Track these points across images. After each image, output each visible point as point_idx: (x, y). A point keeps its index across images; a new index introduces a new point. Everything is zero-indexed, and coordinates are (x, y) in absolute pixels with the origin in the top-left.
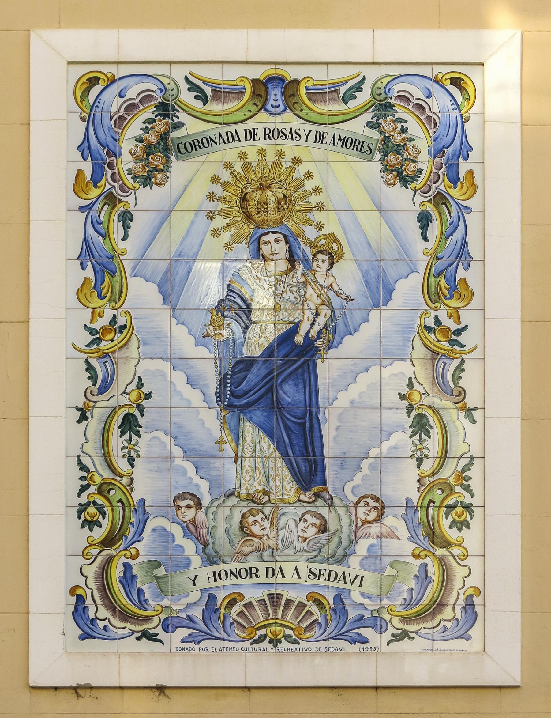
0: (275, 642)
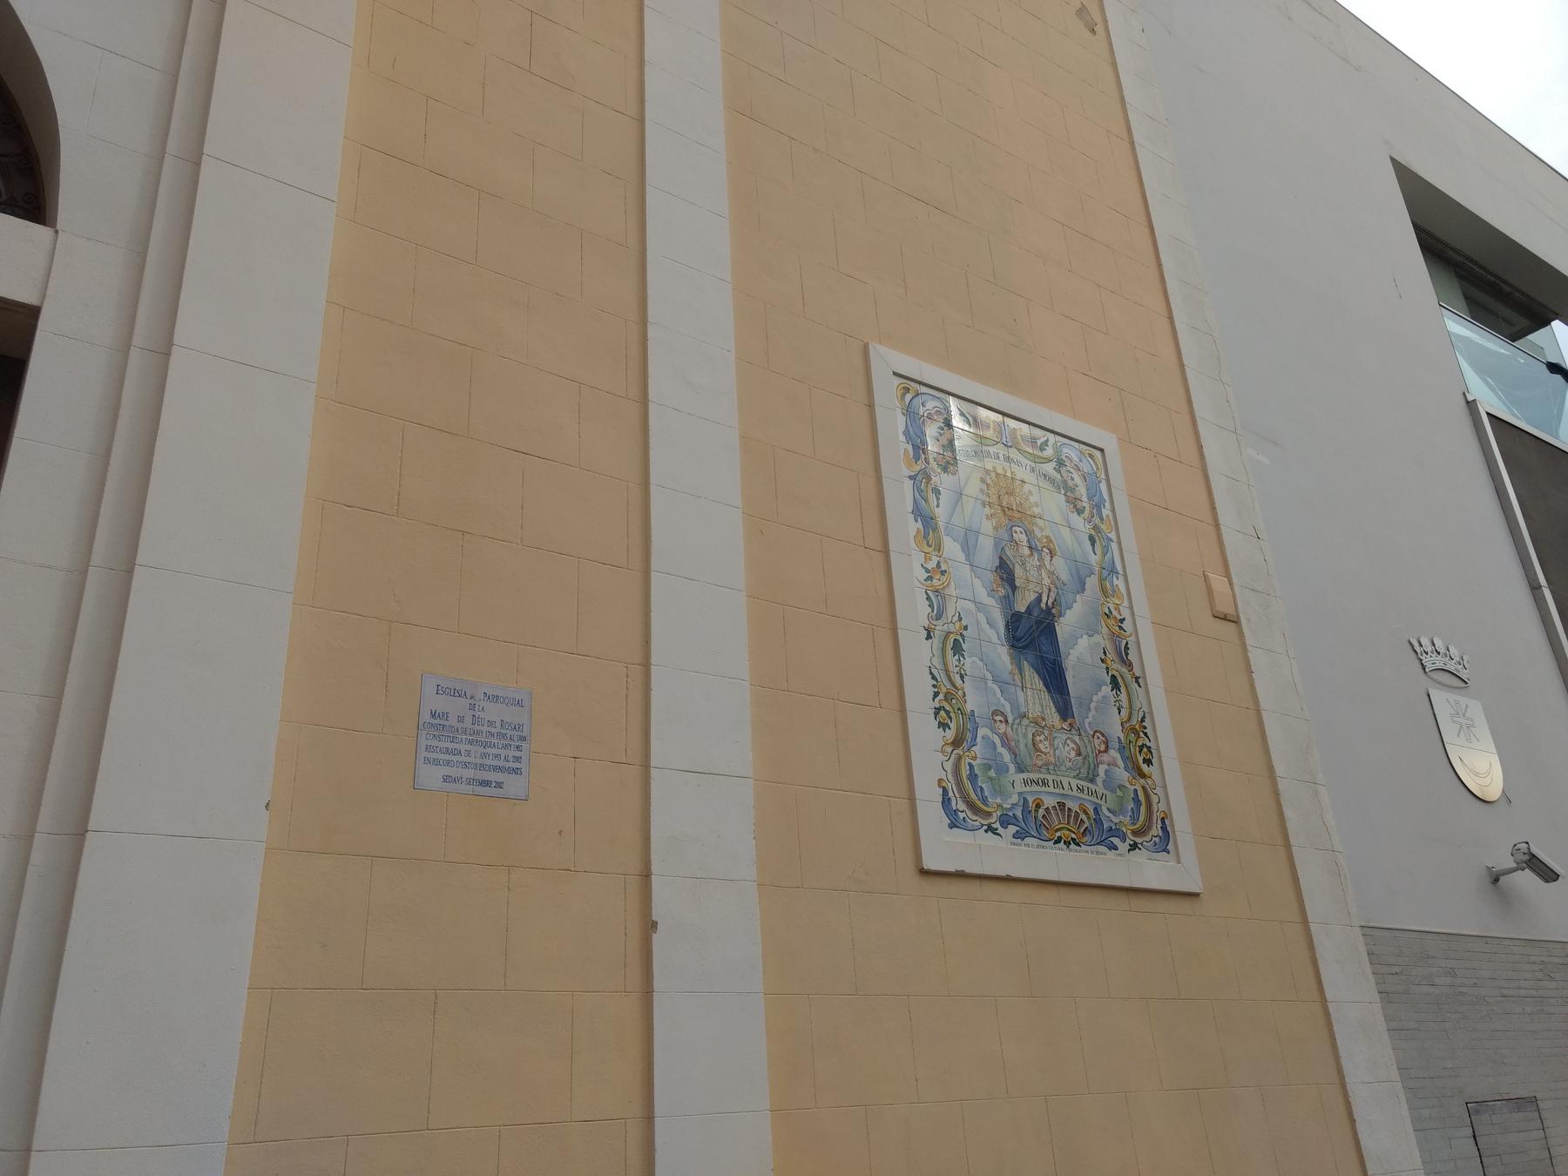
0: (1067, 844)
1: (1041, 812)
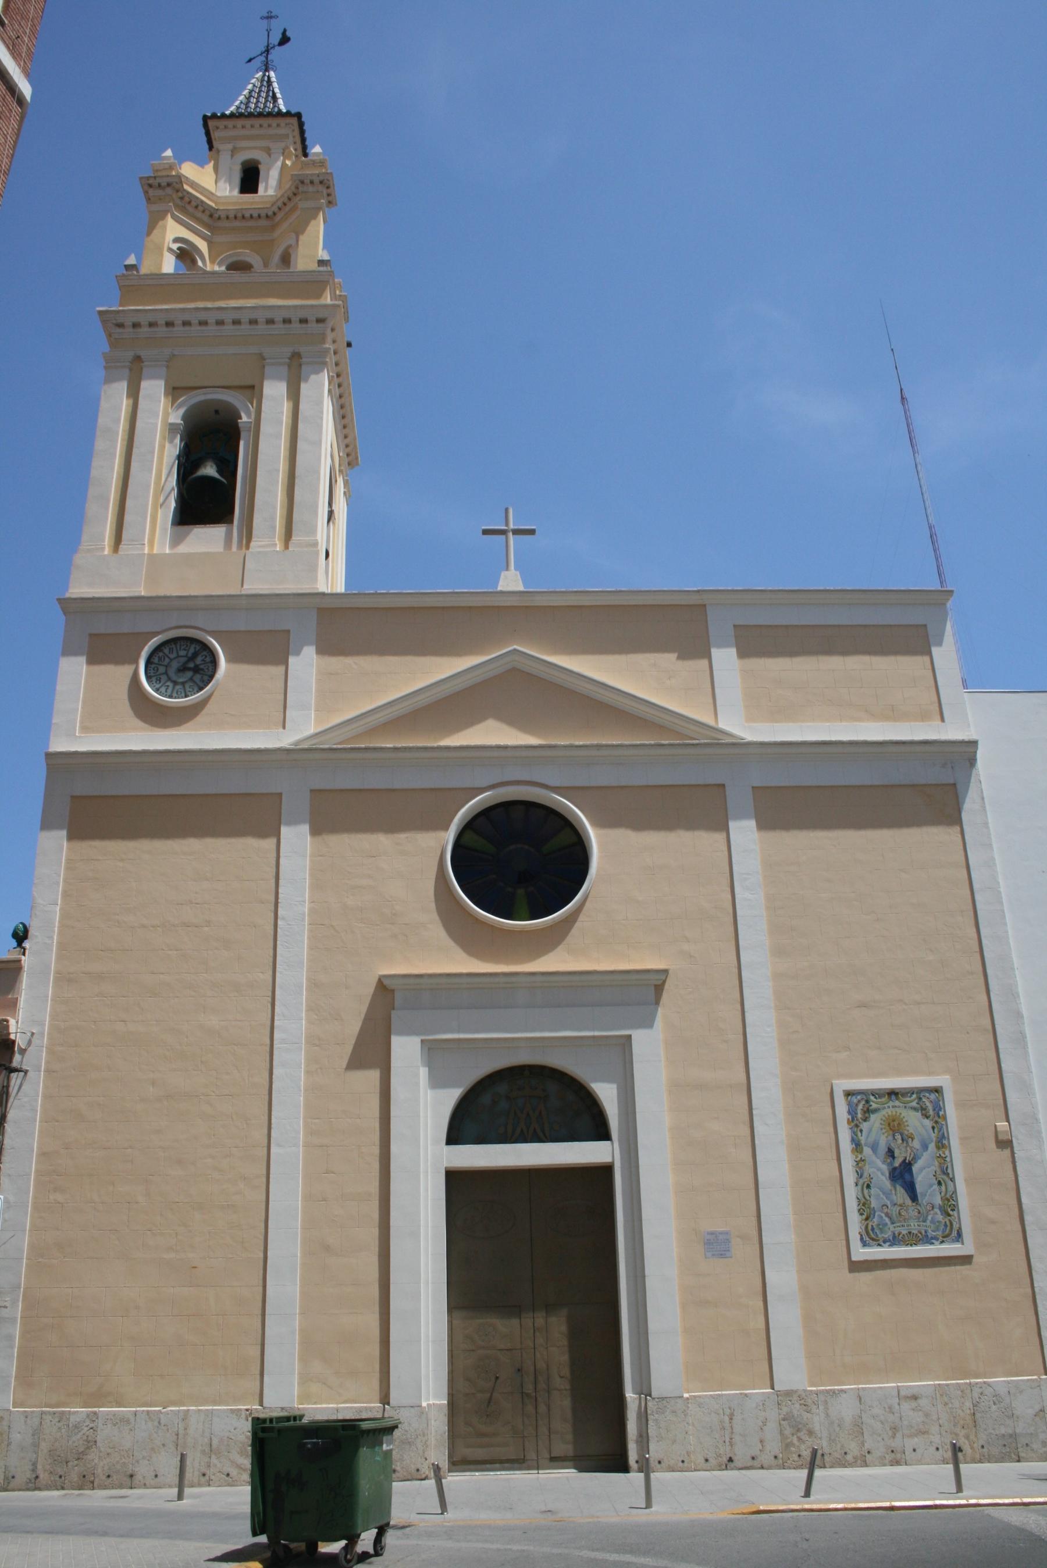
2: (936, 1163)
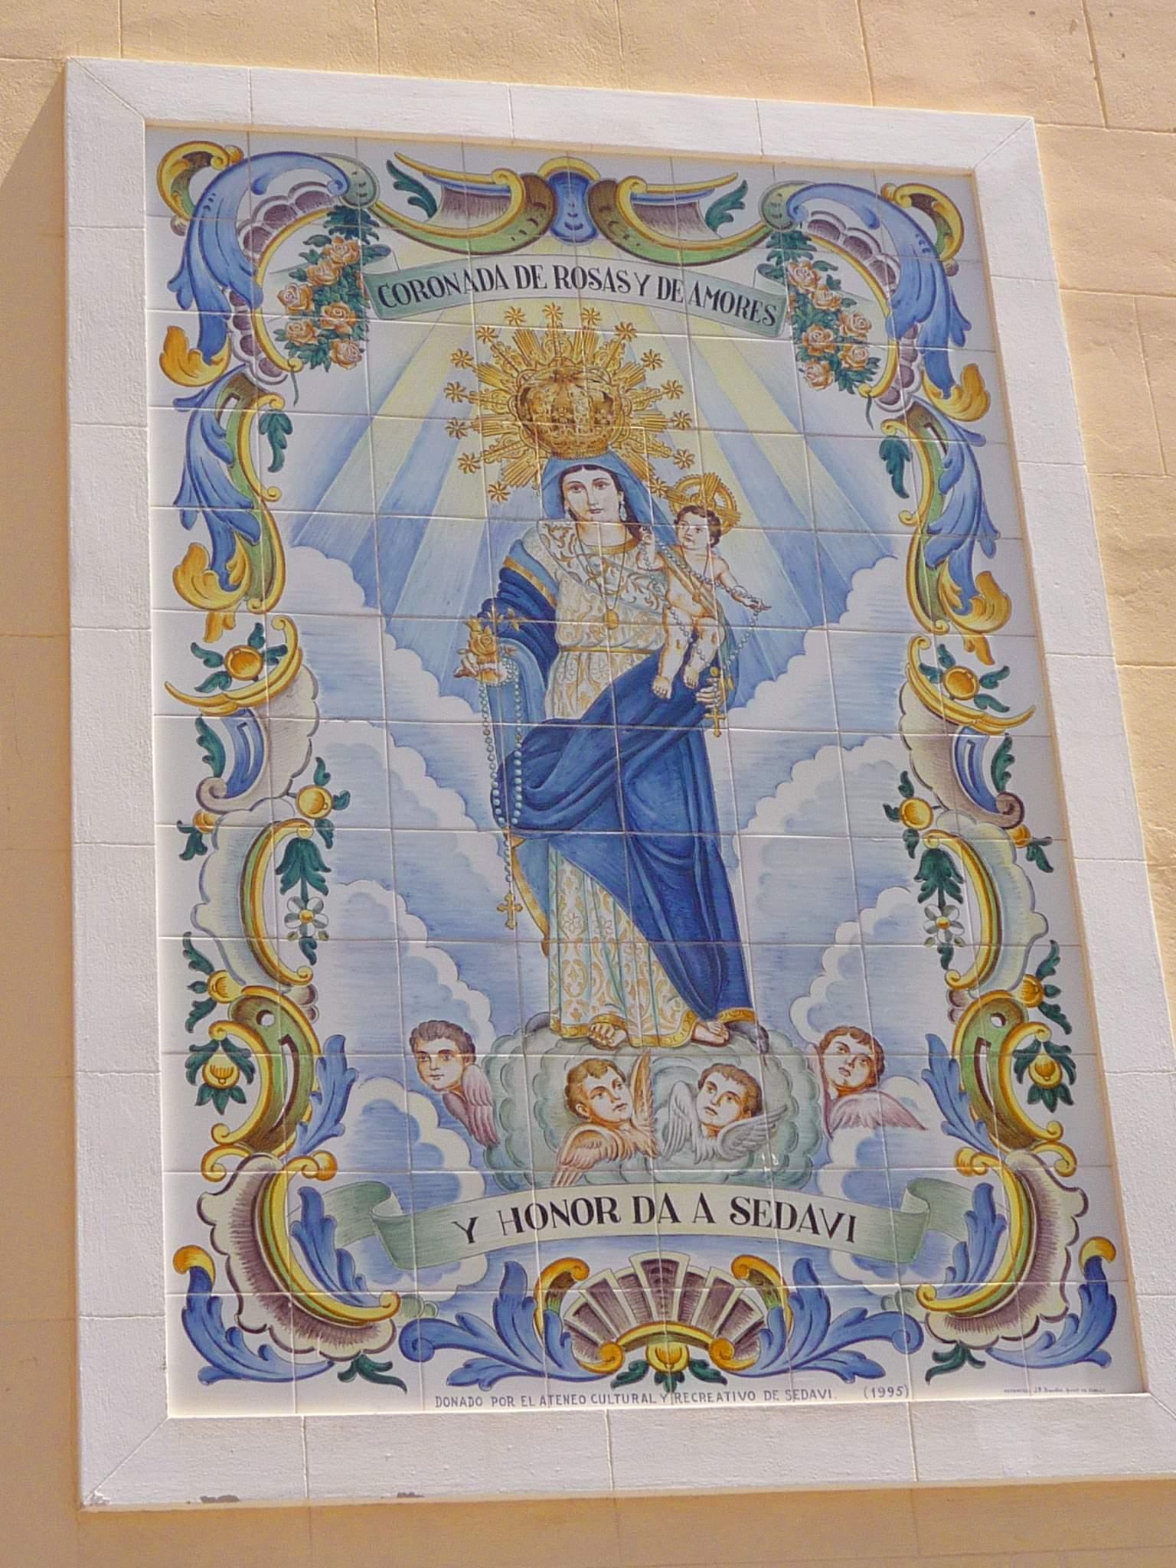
1: (575, 1296)
2: (916, 721)
